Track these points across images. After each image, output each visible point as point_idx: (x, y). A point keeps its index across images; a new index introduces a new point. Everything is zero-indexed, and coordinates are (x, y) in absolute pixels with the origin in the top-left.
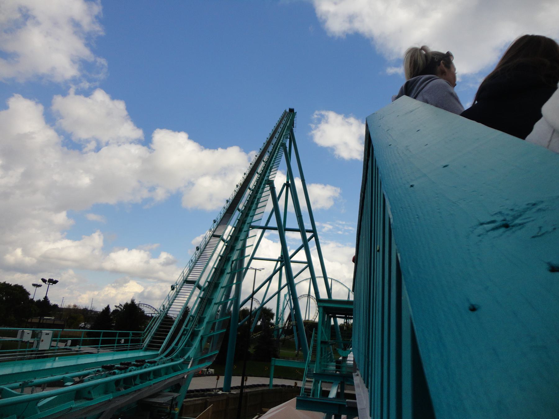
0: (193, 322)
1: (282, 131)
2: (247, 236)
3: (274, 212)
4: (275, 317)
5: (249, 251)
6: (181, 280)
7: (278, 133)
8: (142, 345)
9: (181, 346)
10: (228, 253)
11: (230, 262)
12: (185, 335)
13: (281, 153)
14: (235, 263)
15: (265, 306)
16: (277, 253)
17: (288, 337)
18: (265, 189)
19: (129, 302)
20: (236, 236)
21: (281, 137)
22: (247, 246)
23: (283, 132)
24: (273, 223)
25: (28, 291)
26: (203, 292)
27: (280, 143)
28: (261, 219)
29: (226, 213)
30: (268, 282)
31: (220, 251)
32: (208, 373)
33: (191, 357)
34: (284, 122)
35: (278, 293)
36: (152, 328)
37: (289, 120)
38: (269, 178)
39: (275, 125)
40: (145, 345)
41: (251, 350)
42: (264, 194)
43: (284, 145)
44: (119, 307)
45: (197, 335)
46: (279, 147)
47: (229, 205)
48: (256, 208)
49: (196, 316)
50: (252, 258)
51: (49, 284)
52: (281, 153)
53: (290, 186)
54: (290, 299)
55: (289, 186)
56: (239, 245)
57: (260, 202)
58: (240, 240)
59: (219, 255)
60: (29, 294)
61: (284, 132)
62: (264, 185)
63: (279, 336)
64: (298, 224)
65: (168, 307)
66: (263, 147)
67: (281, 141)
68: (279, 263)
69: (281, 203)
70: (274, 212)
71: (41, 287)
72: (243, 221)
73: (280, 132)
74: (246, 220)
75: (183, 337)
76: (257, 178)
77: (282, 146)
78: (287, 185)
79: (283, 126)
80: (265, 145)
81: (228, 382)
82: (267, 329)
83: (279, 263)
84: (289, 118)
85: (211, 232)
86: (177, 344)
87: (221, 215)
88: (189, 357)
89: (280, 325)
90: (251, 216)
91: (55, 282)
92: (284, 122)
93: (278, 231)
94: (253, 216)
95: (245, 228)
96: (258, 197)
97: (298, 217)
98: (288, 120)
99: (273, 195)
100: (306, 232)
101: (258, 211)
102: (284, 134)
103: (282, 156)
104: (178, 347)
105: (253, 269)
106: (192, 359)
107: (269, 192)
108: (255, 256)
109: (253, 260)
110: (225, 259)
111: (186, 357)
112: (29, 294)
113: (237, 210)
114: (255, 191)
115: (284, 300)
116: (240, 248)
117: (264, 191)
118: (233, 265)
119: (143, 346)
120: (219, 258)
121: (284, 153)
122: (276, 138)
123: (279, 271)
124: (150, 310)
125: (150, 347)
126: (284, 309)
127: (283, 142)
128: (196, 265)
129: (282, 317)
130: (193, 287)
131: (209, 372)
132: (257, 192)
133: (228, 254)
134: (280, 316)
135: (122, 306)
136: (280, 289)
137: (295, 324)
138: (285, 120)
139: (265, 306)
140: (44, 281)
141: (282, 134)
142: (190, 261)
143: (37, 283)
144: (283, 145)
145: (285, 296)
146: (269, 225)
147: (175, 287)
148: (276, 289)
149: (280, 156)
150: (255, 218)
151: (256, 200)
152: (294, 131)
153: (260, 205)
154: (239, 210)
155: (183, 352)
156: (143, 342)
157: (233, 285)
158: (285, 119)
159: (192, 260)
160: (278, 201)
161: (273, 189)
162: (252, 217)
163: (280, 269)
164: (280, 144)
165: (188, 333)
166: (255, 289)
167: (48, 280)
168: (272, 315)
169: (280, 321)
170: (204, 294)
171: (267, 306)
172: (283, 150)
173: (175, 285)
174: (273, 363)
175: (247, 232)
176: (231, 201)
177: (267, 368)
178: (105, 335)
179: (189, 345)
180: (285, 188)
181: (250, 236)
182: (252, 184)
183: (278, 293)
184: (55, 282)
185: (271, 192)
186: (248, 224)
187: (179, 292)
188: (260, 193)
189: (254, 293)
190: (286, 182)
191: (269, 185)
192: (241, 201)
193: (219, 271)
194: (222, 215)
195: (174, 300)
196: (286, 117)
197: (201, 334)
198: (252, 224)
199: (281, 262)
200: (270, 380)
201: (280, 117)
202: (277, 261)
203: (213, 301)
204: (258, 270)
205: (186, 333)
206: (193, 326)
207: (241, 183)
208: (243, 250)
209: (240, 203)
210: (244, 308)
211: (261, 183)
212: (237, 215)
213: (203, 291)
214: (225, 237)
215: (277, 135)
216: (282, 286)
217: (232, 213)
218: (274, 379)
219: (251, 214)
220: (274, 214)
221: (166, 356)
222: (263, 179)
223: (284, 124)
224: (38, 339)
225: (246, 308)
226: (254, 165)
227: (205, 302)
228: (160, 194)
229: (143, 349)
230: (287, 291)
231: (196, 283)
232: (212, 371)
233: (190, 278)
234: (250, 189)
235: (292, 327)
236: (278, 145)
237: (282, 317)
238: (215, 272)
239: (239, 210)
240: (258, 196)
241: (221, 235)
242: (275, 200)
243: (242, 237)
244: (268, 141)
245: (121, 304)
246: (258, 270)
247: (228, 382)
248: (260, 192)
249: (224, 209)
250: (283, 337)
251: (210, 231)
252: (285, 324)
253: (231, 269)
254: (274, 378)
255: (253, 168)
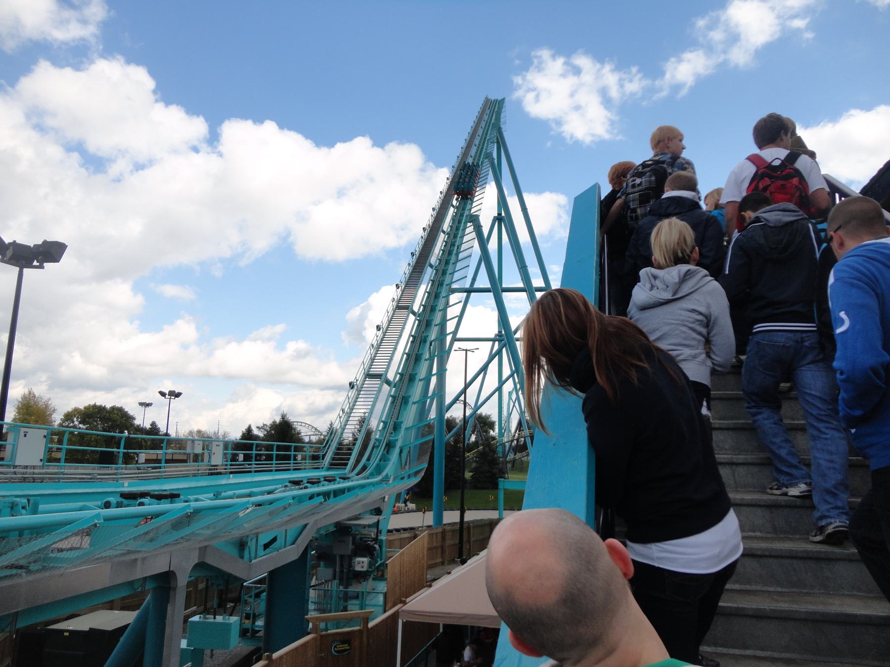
0: (387, 429)
1: (485, 134)
2: (447, 305)
3: (483, 263)
4: (497, 427)
5: (450, 326)
6: (360, 377)
7: (478, 137)
8: (322, 462)
9: (374, 461)
10: (423, 331)
11: (428, 344)
12: (378, 447)
13: (487, 170)
14: (434, 346)
15: (479, 412)
16: (492, 330)
17: (518, 455)
18: (468, 230)
19: (278, 419)
20: (432, 306)
21: (484, 143)
22: (448, 318)
23: (486, 135)
24: (483, 281)
25: (131, 414)
26: (394, 389)
27: (483, 153)
28: (466, 277)
29: (412, 272)
30: (482, 375)
31: (410, 330)
32: (407, 509)
33: (389, 475)
34: (486, 117)
35: (499, 389)
36: (332, 440)
37: (494, 114)
38: (471, 212)
39: (472, 124)
40: (326, 463)
41: (468, 475)
42: (466, 239)
43: (490, 156)
44: (263, 429)
45: (394, 447)
46: (481, 160)
47: (415, 261)
48: (457, 261)
49: (389, 421)
50: (455, 339)
51: (170, 398)
52: (487, 170)
53: (505, 220)
54: (518, 398)
55: (503, 219)
56: (437, 319)
57: (462, 251)
58: (437, 311)
59: (410, 335)
60: (134, 419)
61: (488, 135)
62: (465, 223)
63: (505, 455)
64: (522, 279)
65: (348, 411)
66: (458, 164)
67: (484, 150)
68: (497, 343)
69: (492, 246)
70: (483, 263)
71: (151, 406)
72: (439, 282)
73: (480, 135)
74: (444, 280)
75: (375, 450)
76: (453, 214)
77: (486, 158)
78: (499, 219)
79: (486, 125)
80: (460, 158)
81: (439, 518)
82: (488, 450)
83: (497, 343)
84: (493, 109)
85: (394, 303)
86: (368, 459)
87: (406, 275)
88: (387, 475)
89: (505, 439)
90: (450, 274)
91: (178, 395)
92: (486, 117)
93: (492, 293)
94: (453, 273)
95: (443, 294)
96: (457, 244)
97: (522, 268)
98: (493, 113)
99: (493, 168)
100: (536, 291)
101: (459, 265)
102: (488, 138)
103: (488, 174)
104: (371, 463)
105: (464, 350)
106: (392, 477)
107: (474, 235)
108: (458, 336)
109: (455, 342)
110: (418, 340)
111: (384, 474)
112: (134, 419)
113: (429, 267)
114: (453, 234)
115: (509, 401)
116: (417, 400)
117: (466, 234)
118: (432, 347)
119: (324, 465)
120: (411, 338)
121: (490, 170)
122: (476, 145)
123: (497, 357)
124: (308, 430)
125: (333, 465)
126: (510, 414)
127: (488, 151)
128: (379, 352)
129: (507, 427)
130: (379, 382)
131: (409, 507)
132: (455, 237)
133: (424, 332)
134: (504, 425)
135: (266, 426)
136: (502, 383)
137: (528, 435)
138: (487, 114)
139: (479, 412)
140: (162, 394)
141: (485, 138)
142: (370, 347)
143: (145, 402)
144: (489, 156)
145: (510, 393)
146: (476, 286)
147: (355, 384)
148: (496, 385)
149: (485, 174)
150: (457, 276)
151: (456, 248)
152: (503, 130)
153: (461, 256)
154: (431, 266)
155: (379, 470)
156: (323, 459)
157: (431, 378)
158: (488, 112)
159: (372, 345)
160: (488, 244)
161: (478, 229)
162: (451, 275)
163: (499, 352)
164: (484, 155)
165: (381, 444)
166: (468, 379)
167: (167, 393)
168: (491, 425)
169: (505, 434)
170: (395, 392)
171: (483, 411)
172: (489, 165)
173: (355, 381)
174: (501, 486)
175: (447, 297)
176: (417, 253)
177: (492, 498)
178: (279, 448)
179: (384, 459)
180: (497, 223)
181: (451, 304)
182: (446, 225)
183: (499, 389)
184: (178, 395)
185: (476, 235)
186: (447, 285)
187: (361, 391)
188: (460, 237)
189: (467, 386)
190: (496, 215)
191: (472, 224)
192: (433, 252)
193: (414, 358)
194: (407, 276)
195: (356, 402)
196: (489, 109)
197: (399, 444)
198: (454, 286)
199: (500, 341)
200: (499, 512)
201: (479, 109)
202: (493, 340)
203: (410, 399)
204: (469, 350)
205: (379, 444)
206: (387, 435)
207: (429, 225)
208: (443, 325)
209: (432, 256)
210: (447, 417)
211: (460, 222)
212: (429, 273)
213: (394, 387)
214: (416, 308)
215: (477, 141)
216: (504, 378)
217: (422, 272)
218: (504, 511)
219: (450, 271)
220: (483, 265)
221: (358, 474)
222: (462, 215)
223: (486, 120)
224: (209, 451)
225: (451, 417)
226: (446, 195)
227: (400, 401)
228: (261, 244)
229: (325, 468)
230: (512, 386)
231: (383, 377)
232: (412, 507)
233: (374, 371)
234: (444, 232)
235: (525, 441)
236: (480, 156)
237: (507, 427)
238: (407, 360)
239: (431, 266)
240: (457, 242)
241: (409, 306)
242: (483, 243)
243: (441, 305)
244: (463, 151)
245: (265, 423)
246: (469, 350)
247: (439, 518)
248: (459, 236)
249: (409, 266)
250: (511, 456)
251: (393, 302)
252: (514, 436)
253: (430, 353)
254: (504, 510)
255: (444, 198)
